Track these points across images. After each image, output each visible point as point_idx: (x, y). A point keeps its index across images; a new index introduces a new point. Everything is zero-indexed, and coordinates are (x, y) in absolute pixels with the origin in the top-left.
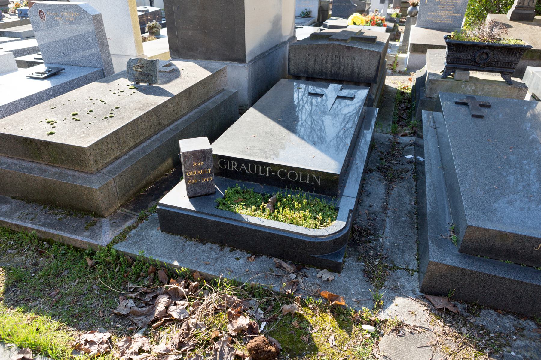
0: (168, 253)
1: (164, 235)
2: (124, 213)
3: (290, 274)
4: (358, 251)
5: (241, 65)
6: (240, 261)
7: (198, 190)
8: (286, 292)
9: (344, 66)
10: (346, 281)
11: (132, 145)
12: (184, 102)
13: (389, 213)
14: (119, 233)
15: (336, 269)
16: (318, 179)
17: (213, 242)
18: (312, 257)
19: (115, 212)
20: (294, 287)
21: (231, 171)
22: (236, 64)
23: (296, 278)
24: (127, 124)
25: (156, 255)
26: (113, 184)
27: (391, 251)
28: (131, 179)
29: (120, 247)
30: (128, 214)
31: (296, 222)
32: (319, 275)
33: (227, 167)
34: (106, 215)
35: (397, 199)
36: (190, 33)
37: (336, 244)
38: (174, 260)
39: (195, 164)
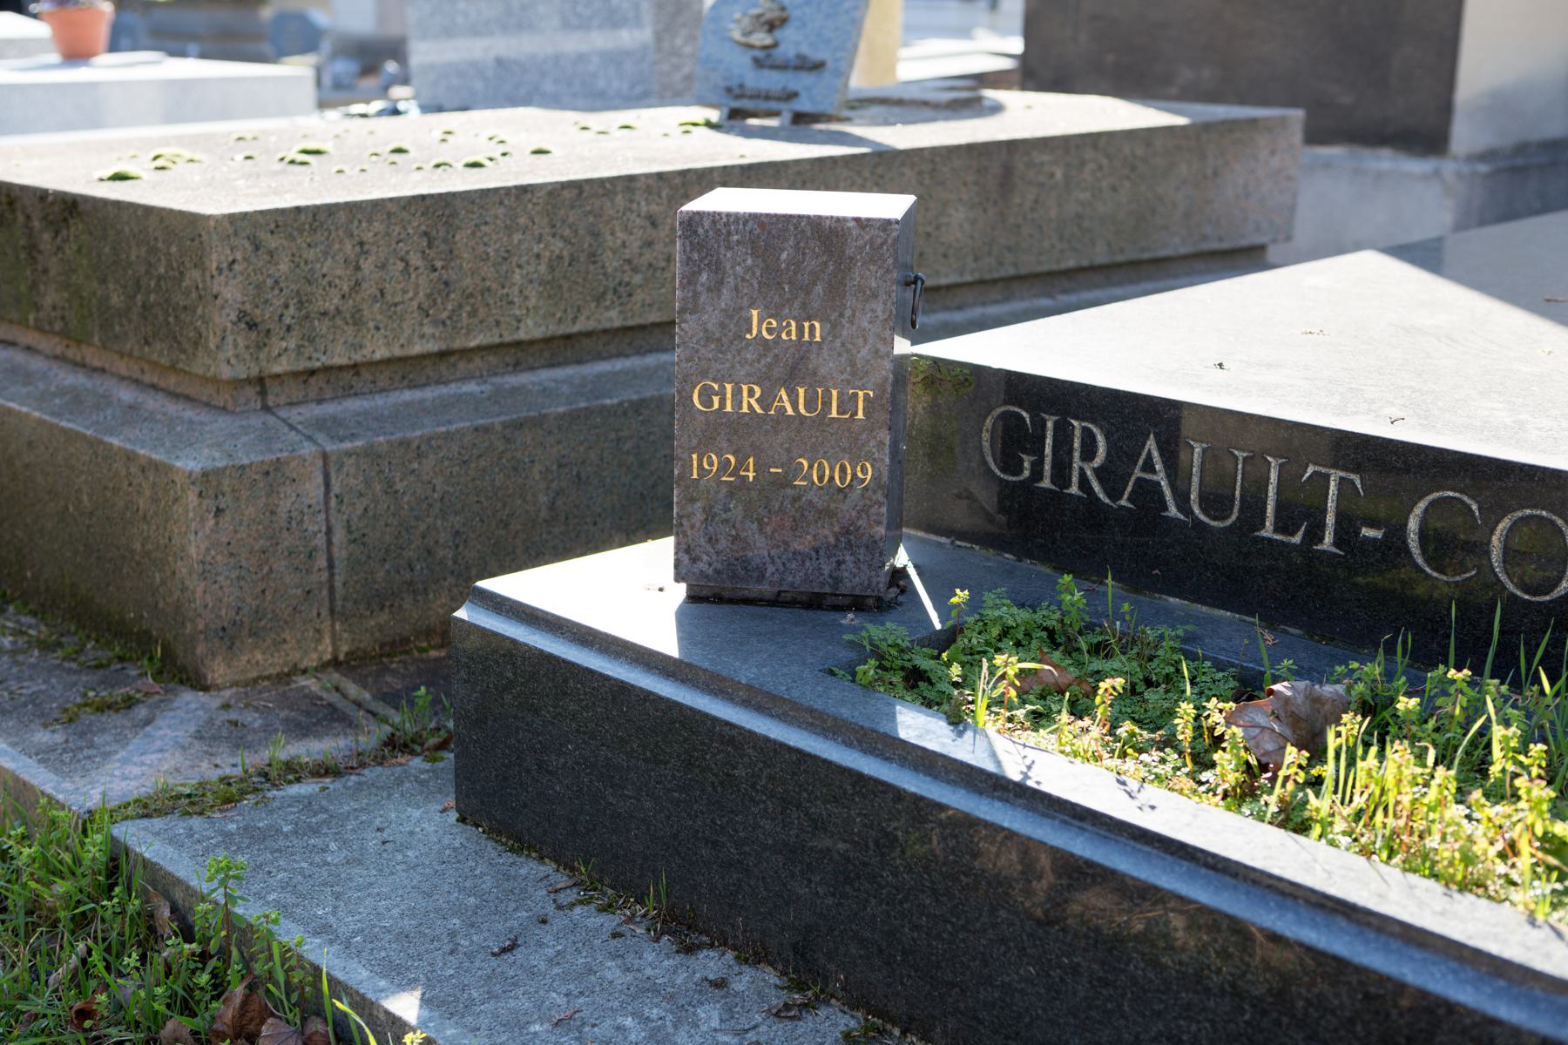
0: (403, 936)
2: (334, 698)
5: (1416, 166)
7: (760, 547)
11: (531, 330)
12: (958, 215)
14: (213, 775)
17: (753, 955)
19: (284, 678)
21: (1057, 498)
22: (1385, 160)
24: (524, 190)
26: (313, 490)
28: (457, 521)
29: (148, 842)
30: (350, 709)
33: (1037, 474)
34: (218, 671)
38: (408, 985)
39: (759, 325)
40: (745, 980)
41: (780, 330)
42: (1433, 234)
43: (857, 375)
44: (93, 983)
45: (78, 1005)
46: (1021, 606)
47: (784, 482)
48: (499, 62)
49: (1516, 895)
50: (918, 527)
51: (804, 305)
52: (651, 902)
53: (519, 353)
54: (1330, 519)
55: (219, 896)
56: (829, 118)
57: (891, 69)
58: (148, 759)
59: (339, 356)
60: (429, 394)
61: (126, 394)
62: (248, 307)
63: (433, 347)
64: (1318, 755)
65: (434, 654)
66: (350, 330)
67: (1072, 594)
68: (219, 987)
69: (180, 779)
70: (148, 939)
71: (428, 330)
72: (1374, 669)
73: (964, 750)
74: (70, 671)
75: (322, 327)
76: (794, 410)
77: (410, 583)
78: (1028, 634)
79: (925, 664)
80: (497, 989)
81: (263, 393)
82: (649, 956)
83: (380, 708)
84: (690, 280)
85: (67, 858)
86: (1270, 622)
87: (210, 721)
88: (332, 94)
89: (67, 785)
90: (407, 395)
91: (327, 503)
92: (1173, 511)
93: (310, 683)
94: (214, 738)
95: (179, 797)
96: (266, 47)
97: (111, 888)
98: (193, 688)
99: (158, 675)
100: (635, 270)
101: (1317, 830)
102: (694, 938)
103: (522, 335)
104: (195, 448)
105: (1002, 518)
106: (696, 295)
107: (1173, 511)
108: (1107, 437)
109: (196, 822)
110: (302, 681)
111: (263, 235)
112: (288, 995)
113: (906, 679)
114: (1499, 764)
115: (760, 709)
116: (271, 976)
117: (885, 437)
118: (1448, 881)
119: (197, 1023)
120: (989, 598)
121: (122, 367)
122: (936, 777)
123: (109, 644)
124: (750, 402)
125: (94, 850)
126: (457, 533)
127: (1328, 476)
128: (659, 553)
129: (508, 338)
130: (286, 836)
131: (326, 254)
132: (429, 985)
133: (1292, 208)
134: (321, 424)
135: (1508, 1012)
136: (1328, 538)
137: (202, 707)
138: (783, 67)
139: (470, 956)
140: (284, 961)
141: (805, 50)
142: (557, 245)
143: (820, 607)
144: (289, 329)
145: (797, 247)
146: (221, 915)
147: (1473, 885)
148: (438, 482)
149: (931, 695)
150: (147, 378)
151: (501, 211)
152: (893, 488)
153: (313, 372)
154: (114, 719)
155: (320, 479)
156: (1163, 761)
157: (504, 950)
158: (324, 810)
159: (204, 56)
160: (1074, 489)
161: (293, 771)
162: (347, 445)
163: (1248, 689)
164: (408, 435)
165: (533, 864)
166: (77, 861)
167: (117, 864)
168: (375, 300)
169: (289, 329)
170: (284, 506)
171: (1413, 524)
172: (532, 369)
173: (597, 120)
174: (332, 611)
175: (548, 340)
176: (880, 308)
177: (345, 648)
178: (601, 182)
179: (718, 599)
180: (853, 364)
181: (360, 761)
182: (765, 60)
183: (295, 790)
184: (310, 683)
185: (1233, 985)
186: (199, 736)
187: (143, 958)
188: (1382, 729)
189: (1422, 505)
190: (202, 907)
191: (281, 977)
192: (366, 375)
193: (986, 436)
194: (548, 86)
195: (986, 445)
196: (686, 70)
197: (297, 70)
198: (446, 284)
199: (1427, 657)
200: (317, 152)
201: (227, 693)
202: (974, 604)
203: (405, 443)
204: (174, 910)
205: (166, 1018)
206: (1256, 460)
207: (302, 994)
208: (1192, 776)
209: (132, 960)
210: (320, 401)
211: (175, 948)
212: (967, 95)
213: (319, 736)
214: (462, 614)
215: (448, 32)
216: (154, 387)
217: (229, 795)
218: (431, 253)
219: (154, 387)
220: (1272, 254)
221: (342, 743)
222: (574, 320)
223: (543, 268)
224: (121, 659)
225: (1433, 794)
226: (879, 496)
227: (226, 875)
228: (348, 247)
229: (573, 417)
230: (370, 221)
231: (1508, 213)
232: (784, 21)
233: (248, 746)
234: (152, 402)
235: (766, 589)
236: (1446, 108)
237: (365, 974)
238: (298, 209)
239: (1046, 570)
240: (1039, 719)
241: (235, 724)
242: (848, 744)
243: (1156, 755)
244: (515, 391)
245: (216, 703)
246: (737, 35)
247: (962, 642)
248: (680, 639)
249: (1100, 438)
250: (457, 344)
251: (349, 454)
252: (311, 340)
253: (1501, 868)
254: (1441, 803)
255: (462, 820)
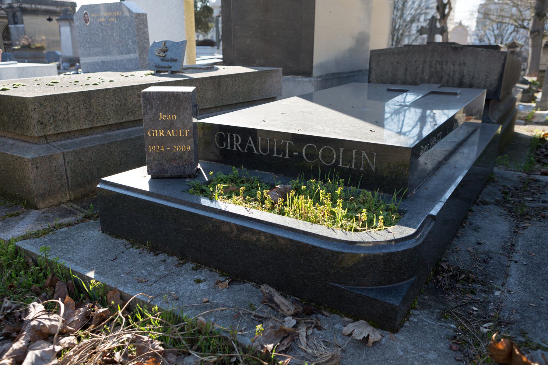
1: (103, 236)
2: (71, 208)
3: (284, 317)
4: (443, 303)
6: (201, 285)
7: (167, 166)
8: (263, 347)
9: (449, 75)
10: (406, 351)
11: (112, 122)
13: (516, 257)
14: (41, 229)
15: (387, 321)
16: (372, 162)
17: (171, 254)
18: (336, 287)
20: (285, 342)
21: (231, 151)
22: (300, 78)
23: (295, 327)
25: (70, 260)
26: (61, 161)
27: (521, 315)
29: (24, 245)
31: (316, 218)
32: (347, 330)
33: (227, 146)
34: (41, 205)
35: (534, 240)
36: (248, 41)
37: (386, 263)
38: (91, 270)
39: (162, 117)
40: (170, 260)
41: (167, 117)
42: (310, 92)
43: (185, 127)
44: (13, 279)
45: (10, 285)
46: (225, 174)
47: (171, 151)
48: (102, 62)
49: (325, 223)
50: (202, 159)
51: (172, 112)
52: (148, 245)
53: (110, 127)
54: (287, 151)
55: (44, 255)
56: (179, 72)
57: (195, 61)
58: (24, 226)
59: (65, 130)
60: (88, 137)
61: (11, 142)
62: (40, 119)
63: (88, 127)
64: (285, 200)
65: (95, 197)
66: (67, 124)
67: (235, 171)
68: (45, 276)
69: (32, 230)
70: (26, 266)
71: (87, 123)
72: (297, 181)
73: (213, 205)
74: (2, 208)
75: (60, 123)
76: (170, 135)
77: (88, 181)
78: (227, 180)
79: (204, 188)
80: (113, 268)
81: (46, 139)
82: (148, 257)
83: (82, 210)
84: (145, 107)
85: (4, 251)
86: (276, 173)
87: (40, 216)
88: (60, 70)
89: (3, 234)
90: (83, 138)
91: (65, 164)
92: (256, 152)
93: (65, 206)
94: (41, 220)
95: (32, 234)
96: (45, 60)
97: (16, 257)
98: (35, 209)
99: (25, 207)
100: (136, 107)
101: (287, 214)
102: (158, 252)
103: (110, 123)
104: (30, 153)
105: (221, 156)
106: (147, 110)
107: (256, 152)
108: (241, 137)
109: (37, 240)
110: (63, 205)
111: (42, 102)
112: (62, 276)
113: (201, 192)
114: (322, 197)
115: (168, 200)
116: (58, 272)
117: (192, 140)
118: (312, 222)
119: (41, 285)
120: (218, 173)
121: (9, 135)
122: (207, 211)
123: (12, 201)
124: (161, 134)
125: (11, 248)
126: (98, 169)
127: (342, 165)
128: (144, 170)
129: (106, 124)
130: (60, 240)
131: (59, 106)
132: (96, 269)
133: (281, 89)
134: (62, 146)
135: (324, 246)
136: (287, 155)
137: (37, 213)
138: (168, 61)
139: (106, 262)
140: (60, 268)
141: (172, 57)
142: (117, 102)
143: (181, 178)
144: (51, 124)
145: (169, 99)
146: (44, 260)
147: (317, 222)
148: (92, 157)
149: (206, 194)
150: (16, 138)
151: (102, 94)
152: (196, 151)
153: (59, 134)
154: (16, 218)
155: (62, 159)
156: (255, 204)
157: (114, 259)
158: (69, 234)
159: (28, 62)
160: (235, 149)
161: (61, 226)
162: (68, 150)
163: (272, 187)
164: (84, 147)
165: (120, 240)
166: (7, 252)
167: (17, 251)
168: (73, 116)
169: (51, 124)
170: (54, 165)
171: (304, 151)
172: (113, 131)
173: (125, 74)
174: (69, 189)
175: (116, 124)
176: (189, 112)
177: (73, 197)
178: (126, 87)
179: (158, 178)
180: (184, 124)
181: (78, 222)
182: (163, 59)
183: (62, 230)
184: (65, 206)
185: (271, 247)
186: (37, 220)
187: (25, 272)
188: (299, 192)
189: (305, 147)
190: (39, 258)
191: (60, 272)
192: (72, 134)
193: (215, 139)
194: (115, 67)
195: (216, 141)
196: (147, 62)
197: (54, 65)
198: (90, 112)
199: (307, 178)
200: (56, 83)
201: (44, 210)
202: (214, 175)
203: (83, 149)
204: (33, 260)
205: (32, 285)
206: (272, 140)
207: (66, 275)
208: (261, 206)
209: (22, 272)
210: (61, 141)
211: (33, 268)
212: (211, 67)
213: (67, 217)
214: (98, 186)
215: (89, 55)
216: (18, 139)
217: (45, 233)
218: (86, 105)
219: (18, 139)
220: (277, 98)
221: (73, 218)
222: (122, 119)
223: (114, 107)
224: (16, 204)
225: (308, 205)
226: (192, 153)
227: (45, 250)
228: (64, 104)
229: (124, 141)
230: (69, 98)
231: (325, 88)
232: (167, 50)
233: (50, 221)
234: (18, 143)
235: (169, 175)
236: (311, 67)
237: (81, 269)
238: (51, 95)
239: (230, 166)
240: (229, 197)
241: (46, 216)
242: (188, 206)
243: (254, 203)
244: (109, 136)
245: (41, 212)
246: (157, 54)
247: (212, 183)
248: (150, 187)
249: (239, 138)
250: (94, 126)
251: (69, 152)
252: (57, 126)
253: (323, 218)
254: (310, 207)
255: (103, 232)
